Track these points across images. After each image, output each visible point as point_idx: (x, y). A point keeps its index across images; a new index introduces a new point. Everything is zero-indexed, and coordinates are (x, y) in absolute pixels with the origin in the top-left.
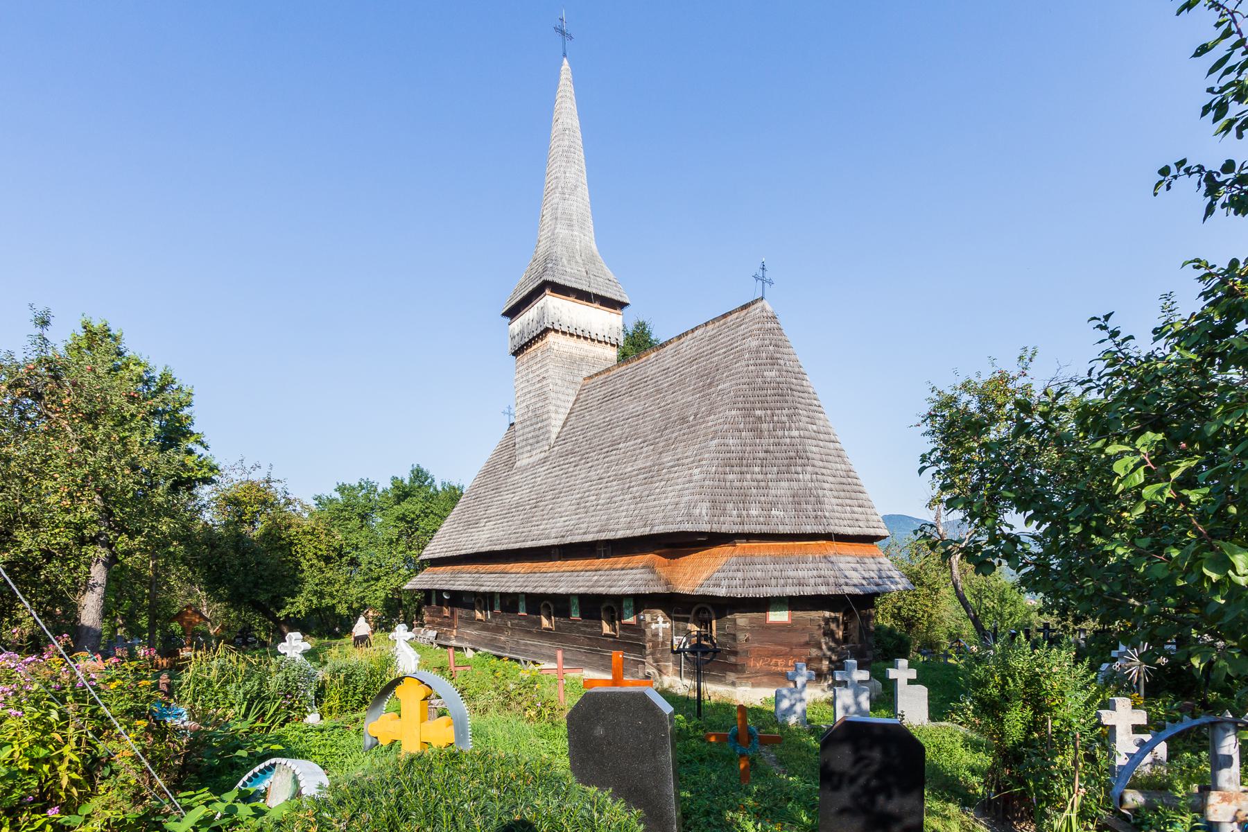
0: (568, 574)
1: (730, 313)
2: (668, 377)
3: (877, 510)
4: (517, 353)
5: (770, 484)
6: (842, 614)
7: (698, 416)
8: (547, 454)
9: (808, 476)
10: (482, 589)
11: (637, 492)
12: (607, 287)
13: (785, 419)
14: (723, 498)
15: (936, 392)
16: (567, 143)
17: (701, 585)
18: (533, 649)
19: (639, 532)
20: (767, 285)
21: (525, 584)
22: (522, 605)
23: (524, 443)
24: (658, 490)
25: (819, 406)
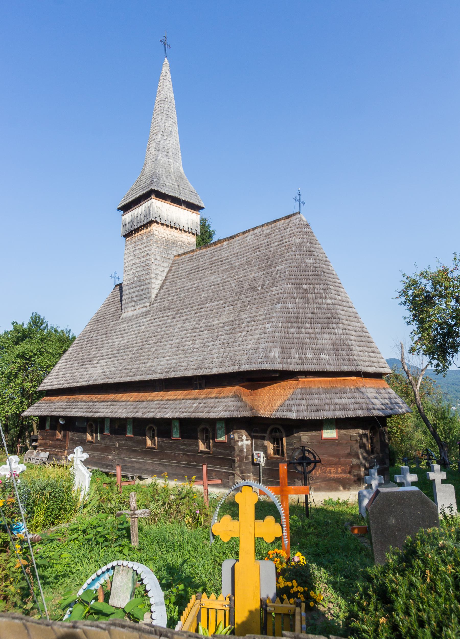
0: (172, 402)
1: (279, 220)
2: (238, 259)
3: (383, 355)
4: (126, 236)
5: (317, 336)
6: (369, 431)
7: (265, 287)
8: (148, 308)
9: (341, 331)
10: (97, 415)
11: (224, 339)
12: (191, 196)
13: (322, 291)
14: (288, 345)
15: (405, 277)
16: (166, 106)
17: (277, 411)
18: (137, 465)
19: (229, 370)
20: (302, 204)
21: (136, 410)
22: (130, 428)
23: (130, 300)
24: (241, 339)
25: (340, 284)
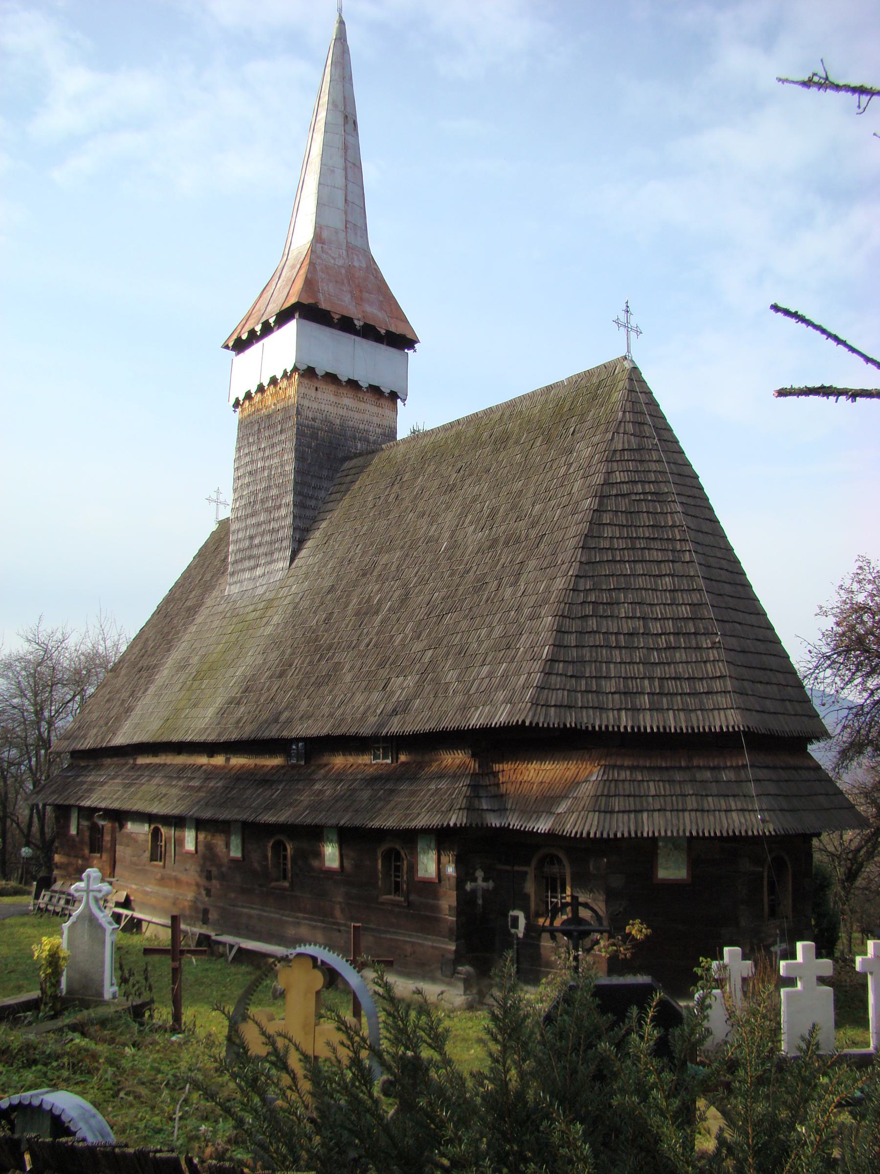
20: (633, 335)
